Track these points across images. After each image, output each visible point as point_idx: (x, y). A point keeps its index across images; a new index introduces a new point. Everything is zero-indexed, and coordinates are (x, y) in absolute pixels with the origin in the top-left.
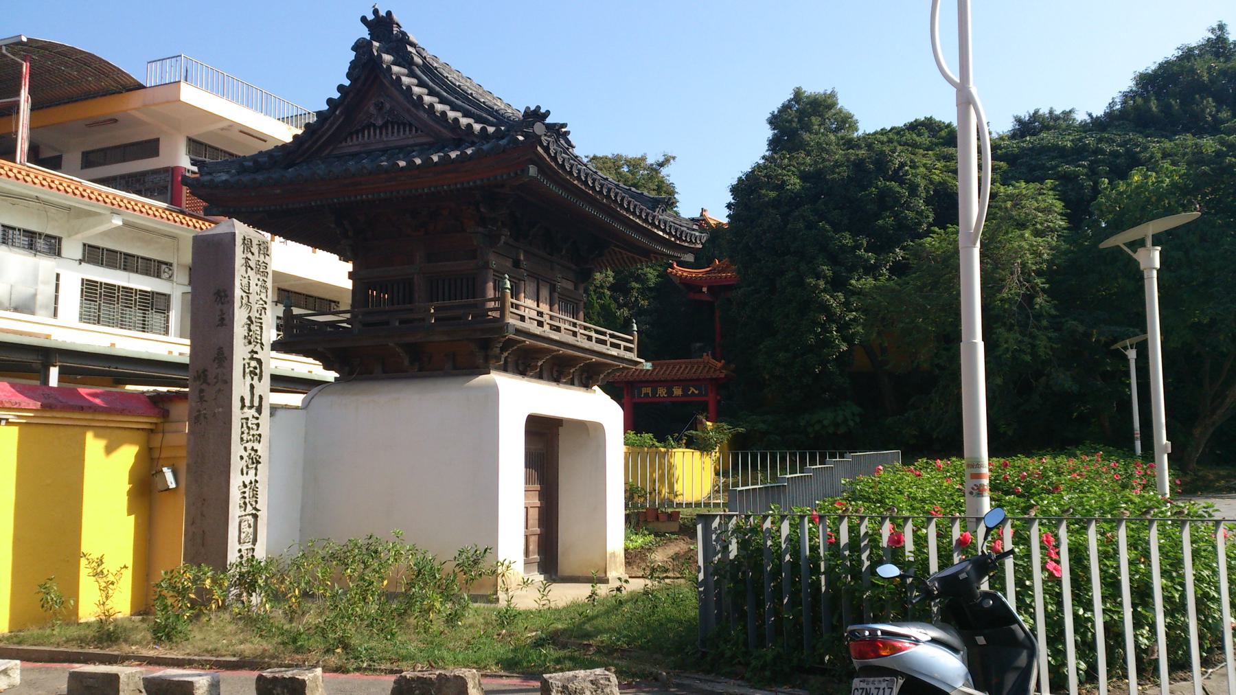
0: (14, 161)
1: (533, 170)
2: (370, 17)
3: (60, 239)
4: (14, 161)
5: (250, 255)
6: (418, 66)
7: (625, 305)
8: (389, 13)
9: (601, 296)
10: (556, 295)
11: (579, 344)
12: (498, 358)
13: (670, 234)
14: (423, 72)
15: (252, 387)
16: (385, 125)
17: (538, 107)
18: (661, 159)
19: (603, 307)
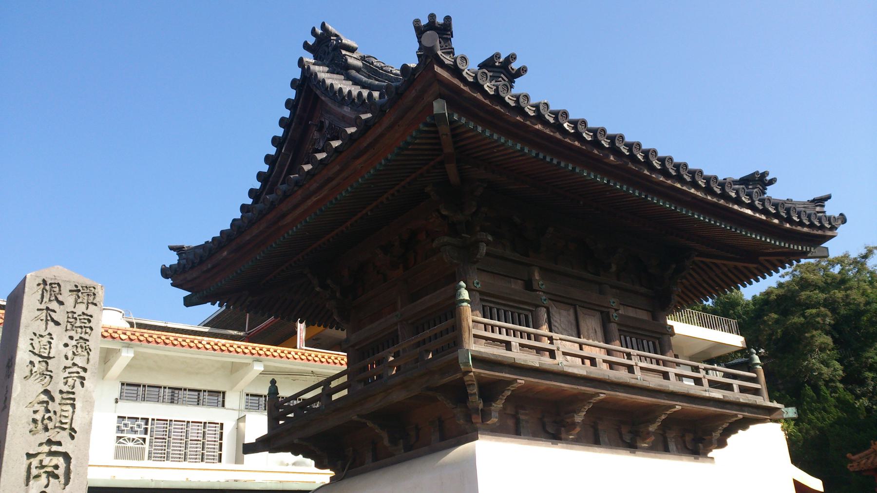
0: (296, 347)
1: (440, 107)
2: (311, 41)
3: (224, 393)
4: (296, 347)
5: (54, 305)
6: (358, 70)
7: (864, 395)
9: (835, 390)
10: (614, 327)
11: (640, 383)
12: (485, 415)
13: (765, 211)
14: (369, 77)
17: (432, 17)
18: (864, 252)
19: (838, 399)
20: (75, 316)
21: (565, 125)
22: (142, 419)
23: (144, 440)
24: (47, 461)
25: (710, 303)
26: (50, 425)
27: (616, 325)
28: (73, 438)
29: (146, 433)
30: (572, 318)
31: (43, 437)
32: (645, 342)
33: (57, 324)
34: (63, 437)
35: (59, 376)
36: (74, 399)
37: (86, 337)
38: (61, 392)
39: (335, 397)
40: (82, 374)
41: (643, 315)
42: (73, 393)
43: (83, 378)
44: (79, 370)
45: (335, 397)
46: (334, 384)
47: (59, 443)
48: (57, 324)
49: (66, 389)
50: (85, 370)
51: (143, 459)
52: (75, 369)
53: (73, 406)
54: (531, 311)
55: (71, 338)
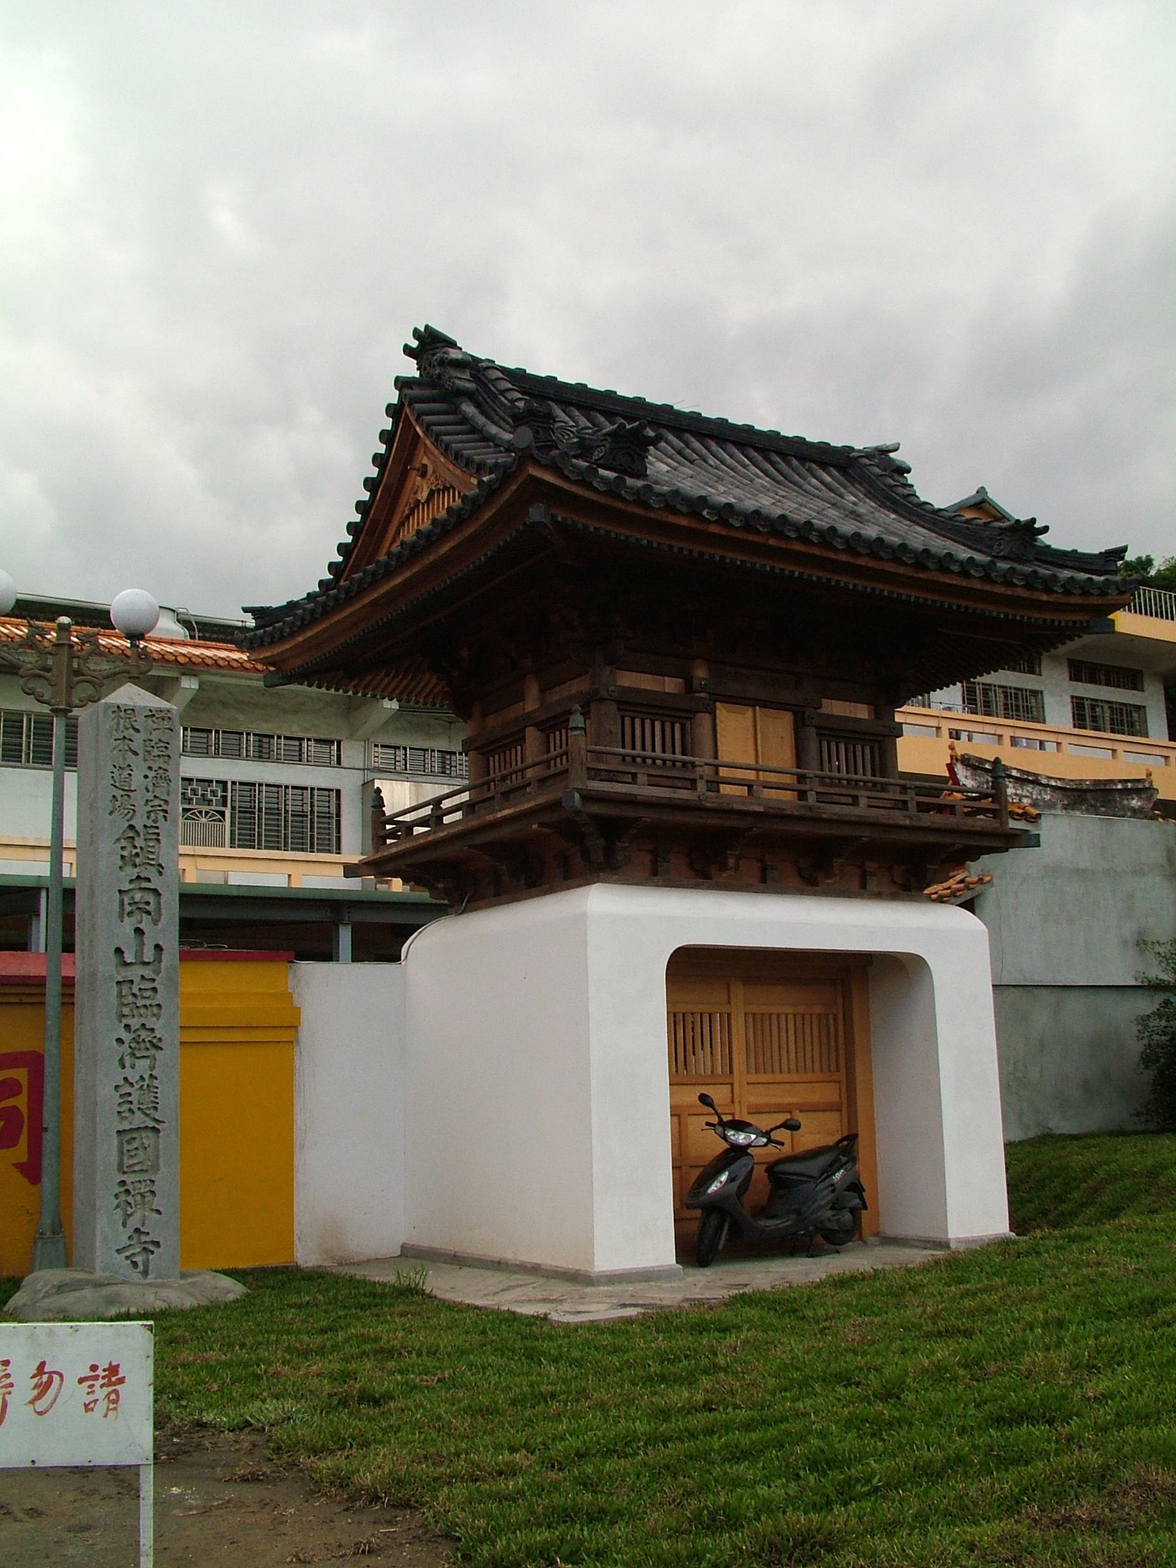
8: (427, 327)
15: (139, 931)
16: (431, 494)
20: (153, 744)
21: (705, 513)
22: (217, 782)
23: (222, 814)
24: (138, 896)
25: (441, 886)
26: (138, 861)
27: (813, 729)
28: (160, 873)
29: (225, 804)
30: (749, 723)
31: (133, 872)
32: (859, 748)
33: (136, 754)
34: (151, 873)
35: (142, 810)
36: (158, 834)
37: (165, 766)
38: (145, 826)
39: (447, 820)
40: (165, 807)
41: (862, 712)
42: (157, 828)
43: (165, 811)
44: (162, 803)
45: (447, 820)
46: (446, 804)
47: (149, 880)
48: (136, 754)
49: (149, 823)
50: (166, 802)
51: (223, 846)
52: (157, 802)
53: (158, 840)
54: (688, 718)
55: (150, 768)
